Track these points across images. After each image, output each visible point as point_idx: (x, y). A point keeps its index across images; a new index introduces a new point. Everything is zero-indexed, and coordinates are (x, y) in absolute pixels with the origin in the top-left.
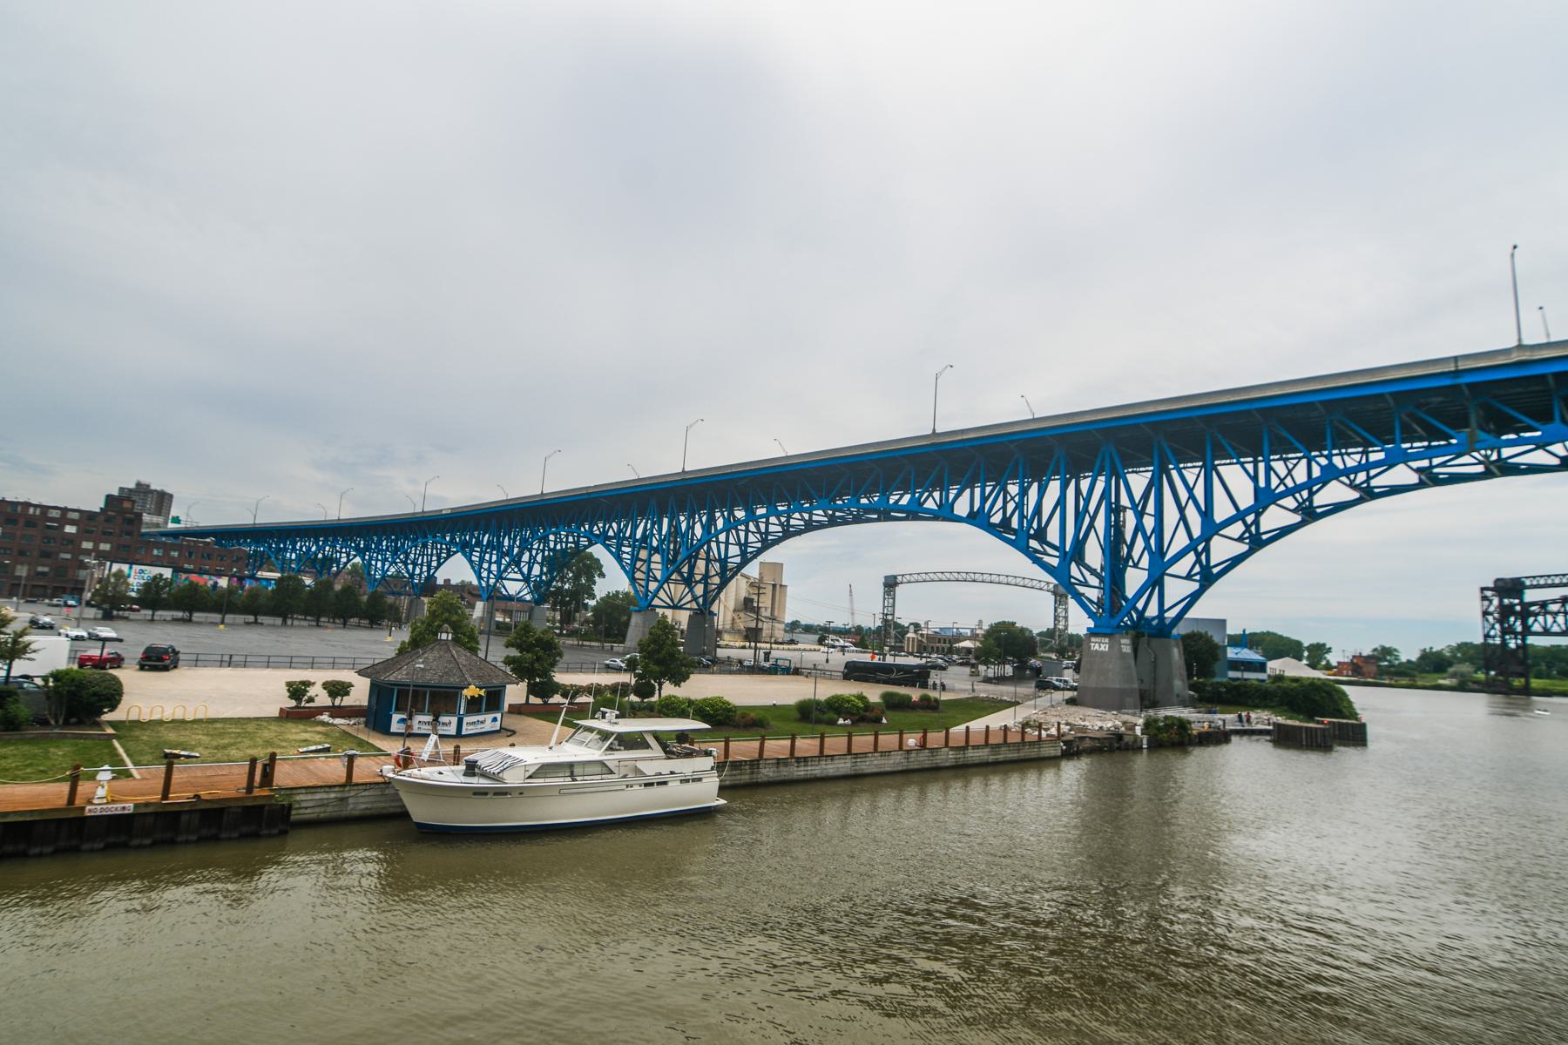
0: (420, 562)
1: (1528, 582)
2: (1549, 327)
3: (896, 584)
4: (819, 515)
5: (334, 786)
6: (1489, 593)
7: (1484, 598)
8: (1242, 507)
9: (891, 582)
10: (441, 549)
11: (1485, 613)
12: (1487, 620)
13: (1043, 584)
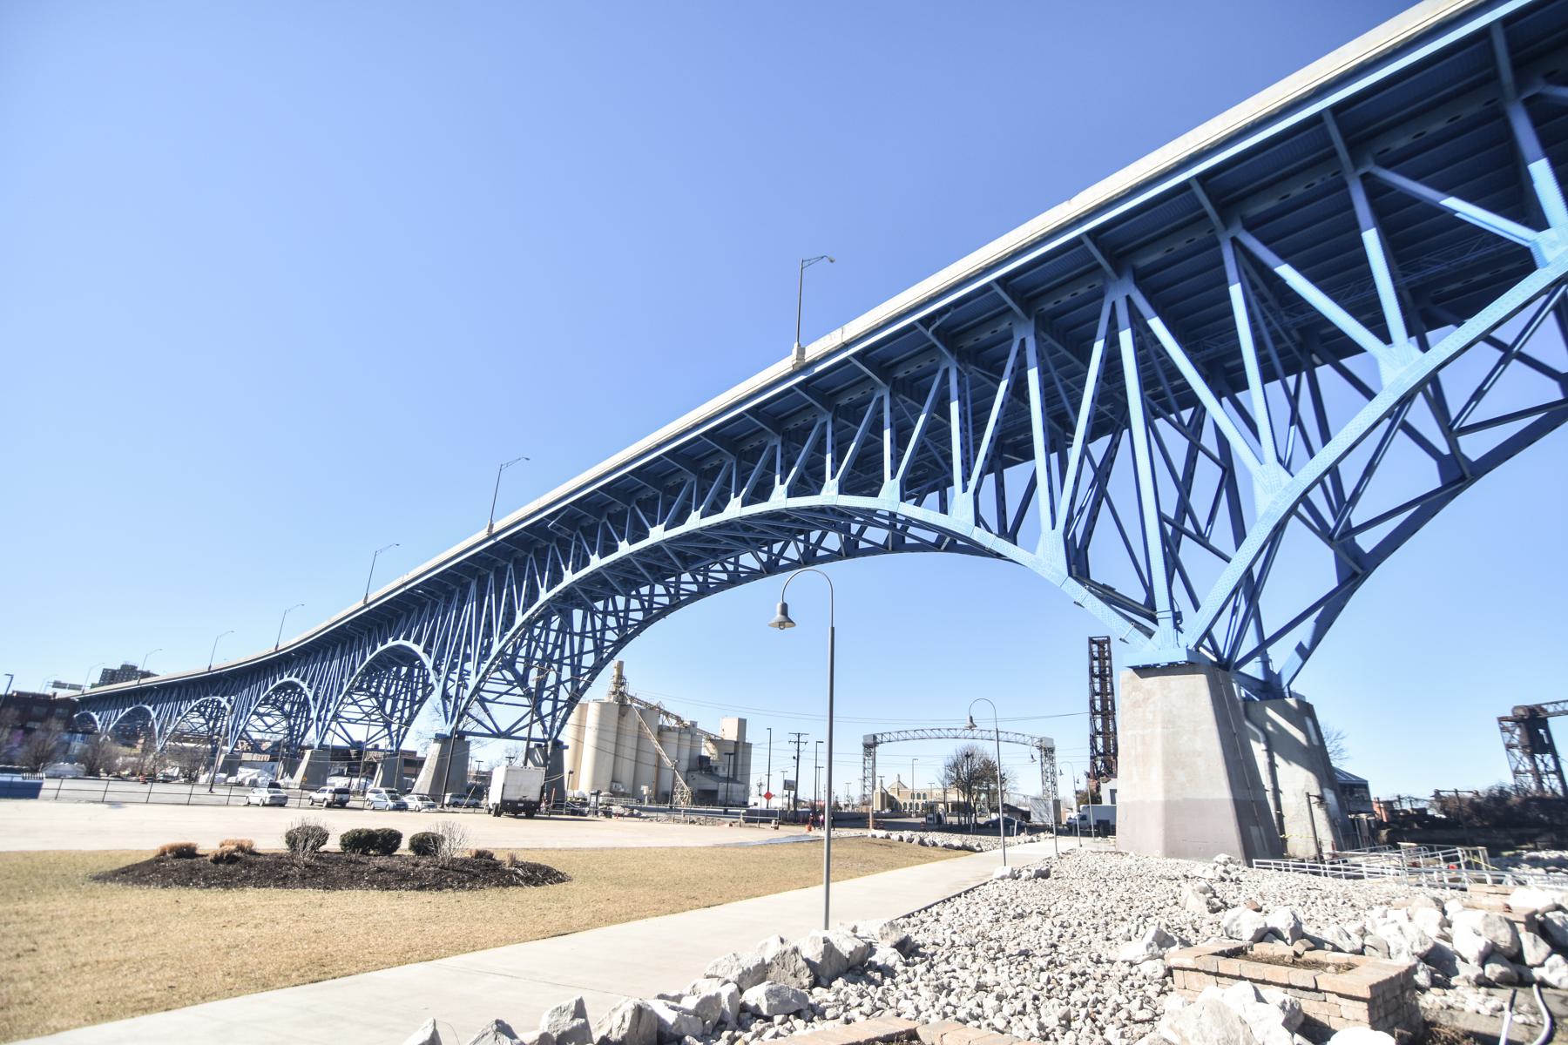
0: (556, 656)
1: (1551, 709)
2: (1280, 982)
3: (875, 744)
4: (748, 560)
5: (958, 848)
6: (1508, 724)
7: (1503, 729)
8: (532, 736)
9: (871, 741)
10: (605, 627)
11: (1509, 747)
12: (1513, 755)
13: (1027, 738)
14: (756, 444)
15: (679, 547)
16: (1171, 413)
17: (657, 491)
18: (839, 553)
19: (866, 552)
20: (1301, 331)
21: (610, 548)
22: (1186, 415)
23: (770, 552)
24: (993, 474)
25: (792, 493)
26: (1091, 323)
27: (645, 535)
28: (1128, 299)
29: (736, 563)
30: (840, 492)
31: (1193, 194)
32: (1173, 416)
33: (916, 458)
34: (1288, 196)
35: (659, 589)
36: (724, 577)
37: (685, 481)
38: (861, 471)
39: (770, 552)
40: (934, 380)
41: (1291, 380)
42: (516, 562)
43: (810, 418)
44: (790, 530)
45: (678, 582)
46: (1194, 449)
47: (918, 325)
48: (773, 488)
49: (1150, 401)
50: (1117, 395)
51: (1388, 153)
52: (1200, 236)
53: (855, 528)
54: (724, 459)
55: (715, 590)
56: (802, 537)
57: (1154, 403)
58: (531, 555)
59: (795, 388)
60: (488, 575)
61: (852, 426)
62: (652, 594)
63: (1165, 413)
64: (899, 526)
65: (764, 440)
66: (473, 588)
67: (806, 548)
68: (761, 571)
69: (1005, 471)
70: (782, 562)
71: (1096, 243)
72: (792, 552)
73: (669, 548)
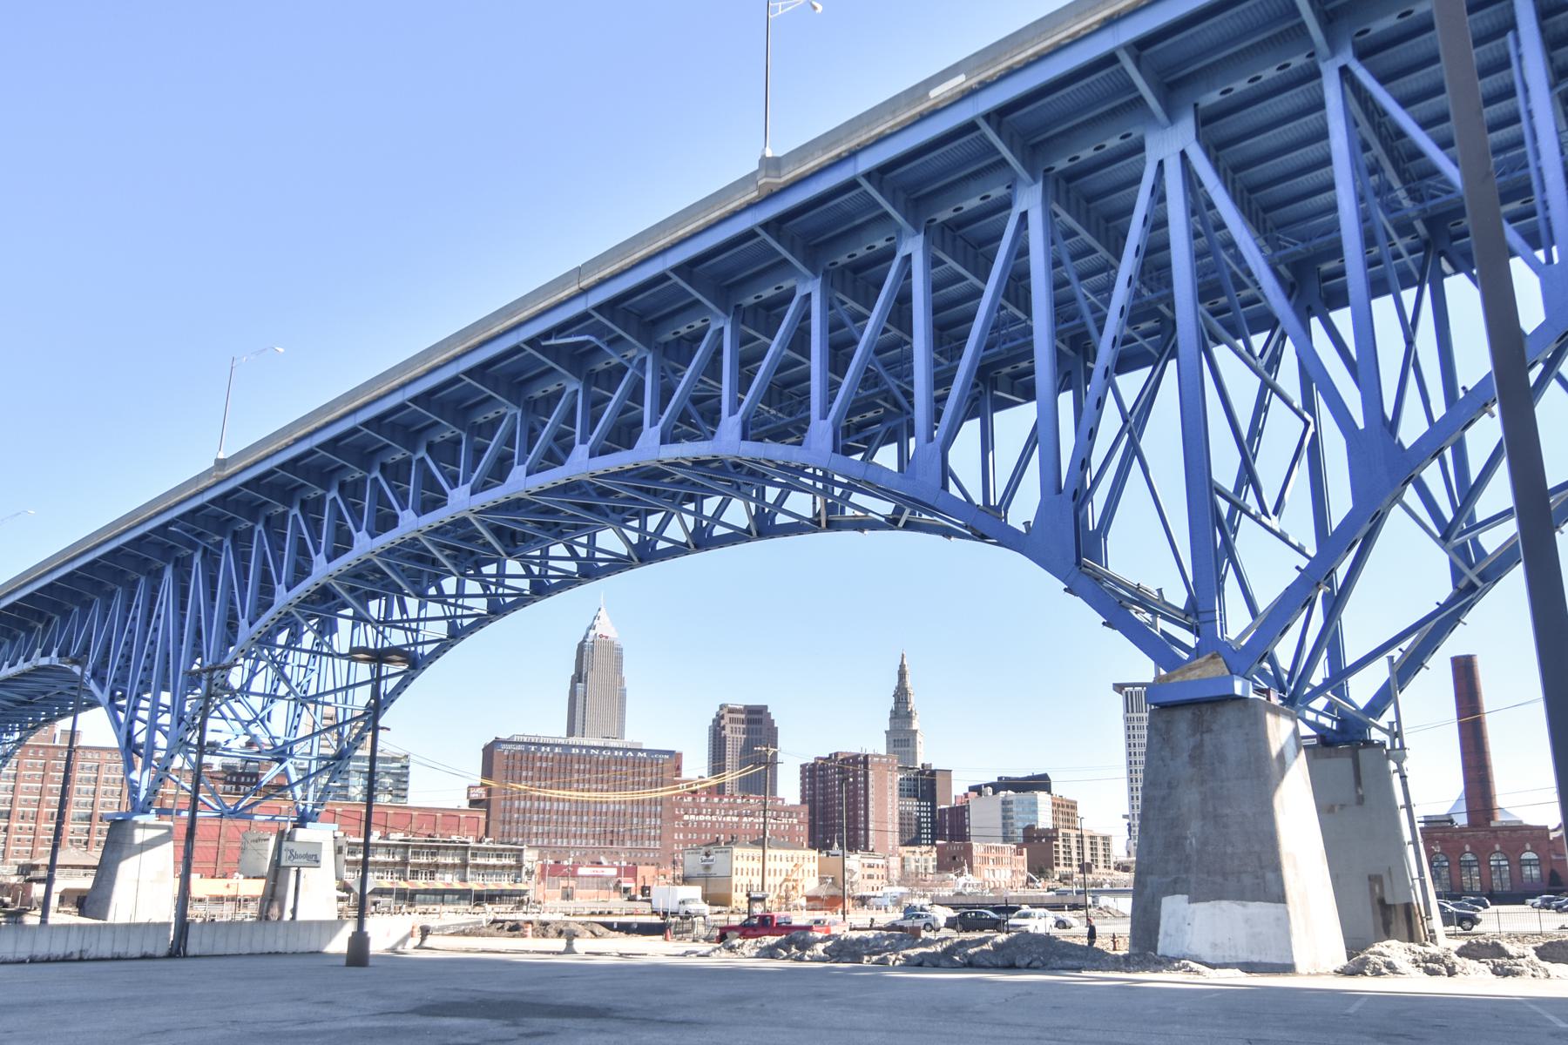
4: (609, 541)
14: (768, 293)
15: (498, 519)
16: (1237, 338)
17: (458, 431)
18: (748, 531)
19: (787, 530)
20: (1429, 222)
21: (386, 522)
22: (1258, 341)
23: (642, 529)
24: (1071, 392)
25: (668, 438)
26: (1128, 191)
27: (439, 502)
28: (1183, 155)
29: (591, 545)
30: (744, 437)
31: (983, 135)
32: (1240, 343)
33: (982, 354)
34: (1367, 31)
35: (513, 566)
36: (572, 566)
37: (564, 390)
38: (780, 410)
39: (642, 529)
40: (786, 311)
41: (1409, 296)
42: (236, 537)
43: (698, 324)
44: (674, 495)
45: (545, 556)
46: (1268, 387)
47: (759, 231)
48: (641, 431)
49: (1208, 316)
50: (1162, 307)
51: (1232, 93)
52: (1298, 61)
53: (772, 494)
54: (564, 383)
55: (558, 588)
56: (691, 507)
57: (1214, 321)
58: (296, 511)
59: (759, 231)
60: (191, 557)
61: (764, 339)
62: (501, 575)
63: (1231, 339)
64: (838, 491)
65: (1136, 133)
66: (168, 575)
67: (698, 524)
68: (629, 557)
69: (995, 415)
70: (661, 545)
71: (1137, 62)
72: (676, 531)
73: (482, 522)
